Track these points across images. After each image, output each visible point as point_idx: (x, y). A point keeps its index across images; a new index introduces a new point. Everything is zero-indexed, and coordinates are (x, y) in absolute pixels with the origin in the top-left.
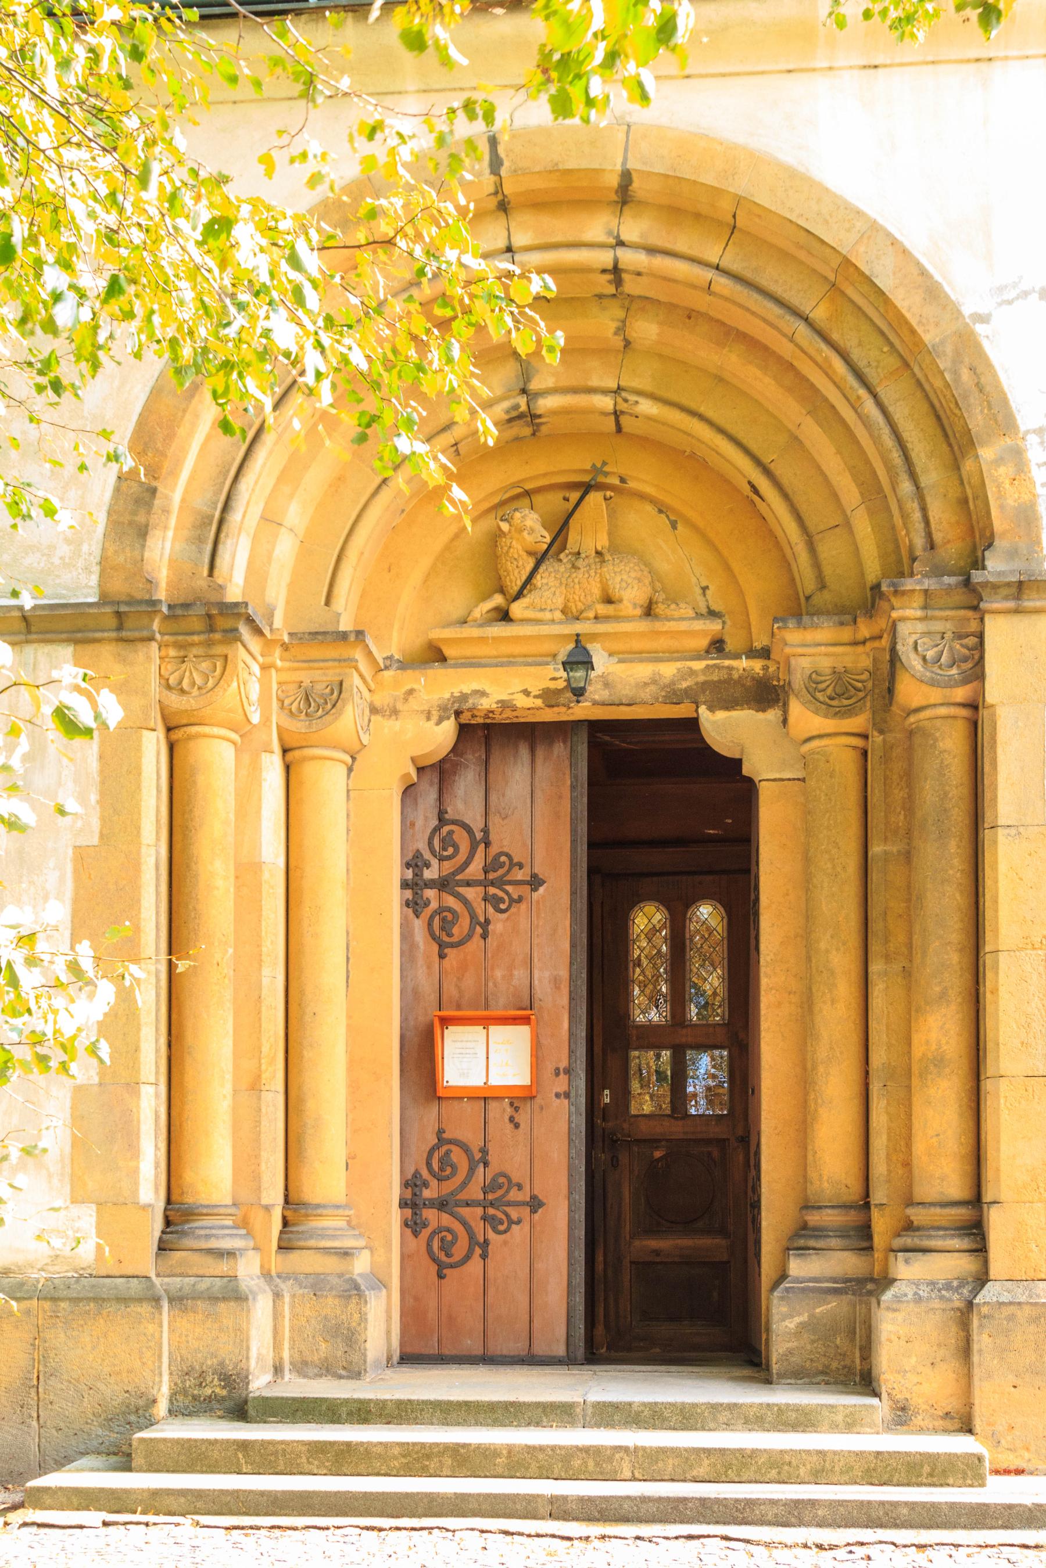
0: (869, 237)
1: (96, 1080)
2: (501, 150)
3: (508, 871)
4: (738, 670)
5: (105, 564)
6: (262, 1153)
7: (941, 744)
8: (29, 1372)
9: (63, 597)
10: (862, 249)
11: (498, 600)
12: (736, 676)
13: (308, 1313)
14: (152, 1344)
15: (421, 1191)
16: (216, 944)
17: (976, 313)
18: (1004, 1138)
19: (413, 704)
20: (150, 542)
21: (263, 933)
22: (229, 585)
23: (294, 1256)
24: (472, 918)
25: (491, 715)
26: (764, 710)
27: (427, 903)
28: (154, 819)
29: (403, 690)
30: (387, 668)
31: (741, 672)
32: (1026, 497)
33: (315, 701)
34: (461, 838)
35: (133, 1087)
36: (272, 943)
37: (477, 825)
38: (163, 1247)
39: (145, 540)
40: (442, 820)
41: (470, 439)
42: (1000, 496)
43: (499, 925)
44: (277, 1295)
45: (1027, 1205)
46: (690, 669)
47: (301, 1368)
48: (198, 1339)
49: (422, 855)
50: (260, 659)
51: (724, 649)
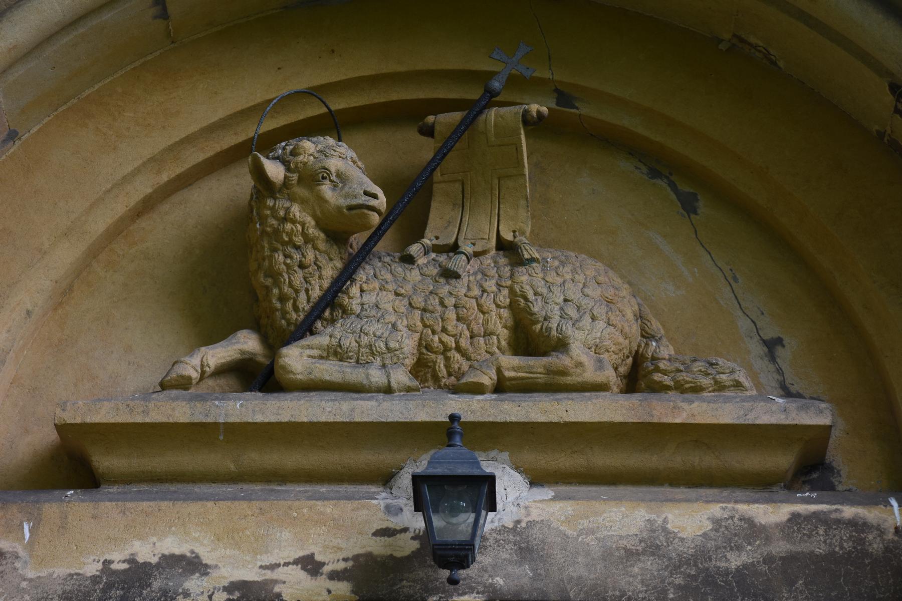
12: (876, 547)
31: (890, 536)
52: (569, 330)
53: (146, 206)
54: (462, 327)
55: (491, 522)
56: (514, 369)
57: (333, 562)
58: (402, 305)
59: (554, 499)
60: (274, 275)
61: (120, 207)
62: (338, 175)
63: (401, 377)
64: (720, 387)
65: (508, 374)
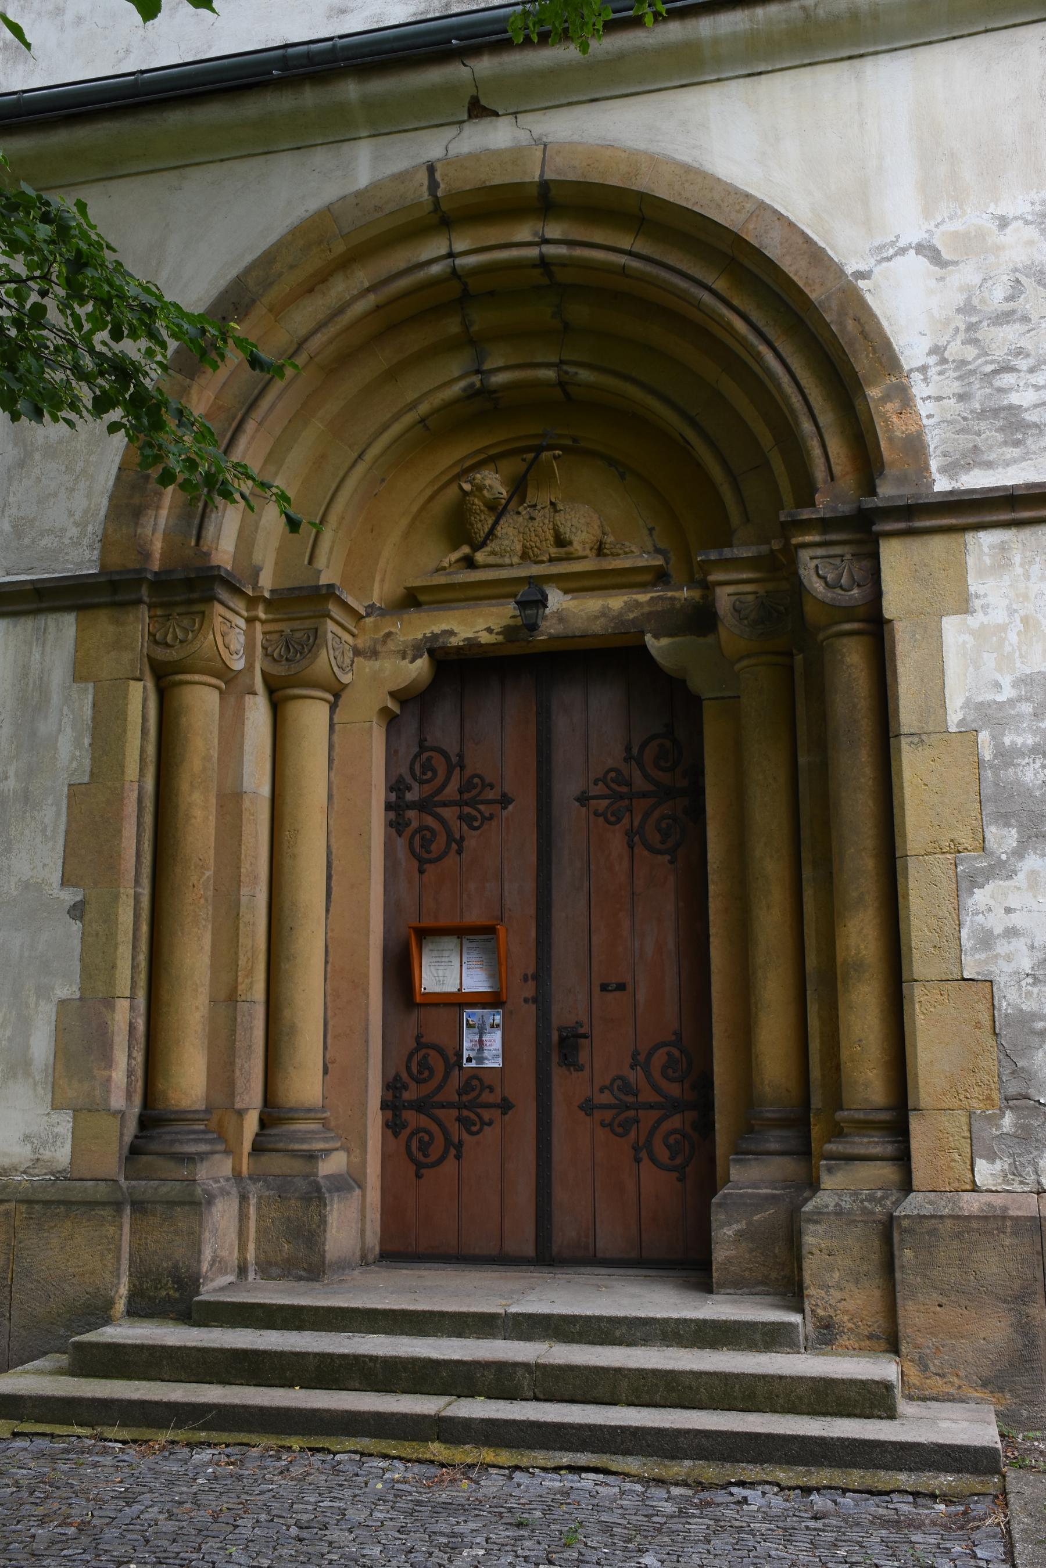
0: (758, 216)
1: (78, 995)
2: (438, 176)
3: (480, 792)
4: (680, 600)
5: (106, 544)
6: (237, 1060)
7: (848, 659)
8: (4, 1271)
9: (71, 570)
10: (751, 226)
11: (466, 550)
12: (678, 606)
13: (273, 1214)
14: (112, 1246)
15: (401, 1094)
16: (193, 867)
17: (857, 271)
18: (921, 1044)
19: (391, 645)
20: (143, 520)
21: (243, 856)
22: (213, 552)
23: (266, 1159)
24: (448, 836)
25: (461, 651)
26: (705, 636)
27: (408, 824)
28: (137, 758)
29: (382, 633)
30: (368, 615)
31: (683, 601)
32: (913, 429)
33: (293, 646)
34: (440, 764)
35: (109, 1002)
36: (251, 864)
37: (453, 750)
38: (135, 1151)
39: (138, 519)
40: (422, 747)
41: (435, 415)
42: (889, 430)
43: (472, 841)
44: (244, 1198)
45: (948, 1112)
46: (636, 601)
47: (265, 1270)
48: (157, 1242)
49: (404, 779)
50: (245, 614)
51: (670, 582)
52: (573, 537)
53: (431, 498)
54: (537, 538)
55: (547, 611)
56: (556, 553)
57: (497, 628)
58: (515, 532)
59: (571, 599)
60: (472, 525)
61: (421, 501)
62: (490, 486)
63: (516, 560)
64: (626, 553)
65: (553, 555)
